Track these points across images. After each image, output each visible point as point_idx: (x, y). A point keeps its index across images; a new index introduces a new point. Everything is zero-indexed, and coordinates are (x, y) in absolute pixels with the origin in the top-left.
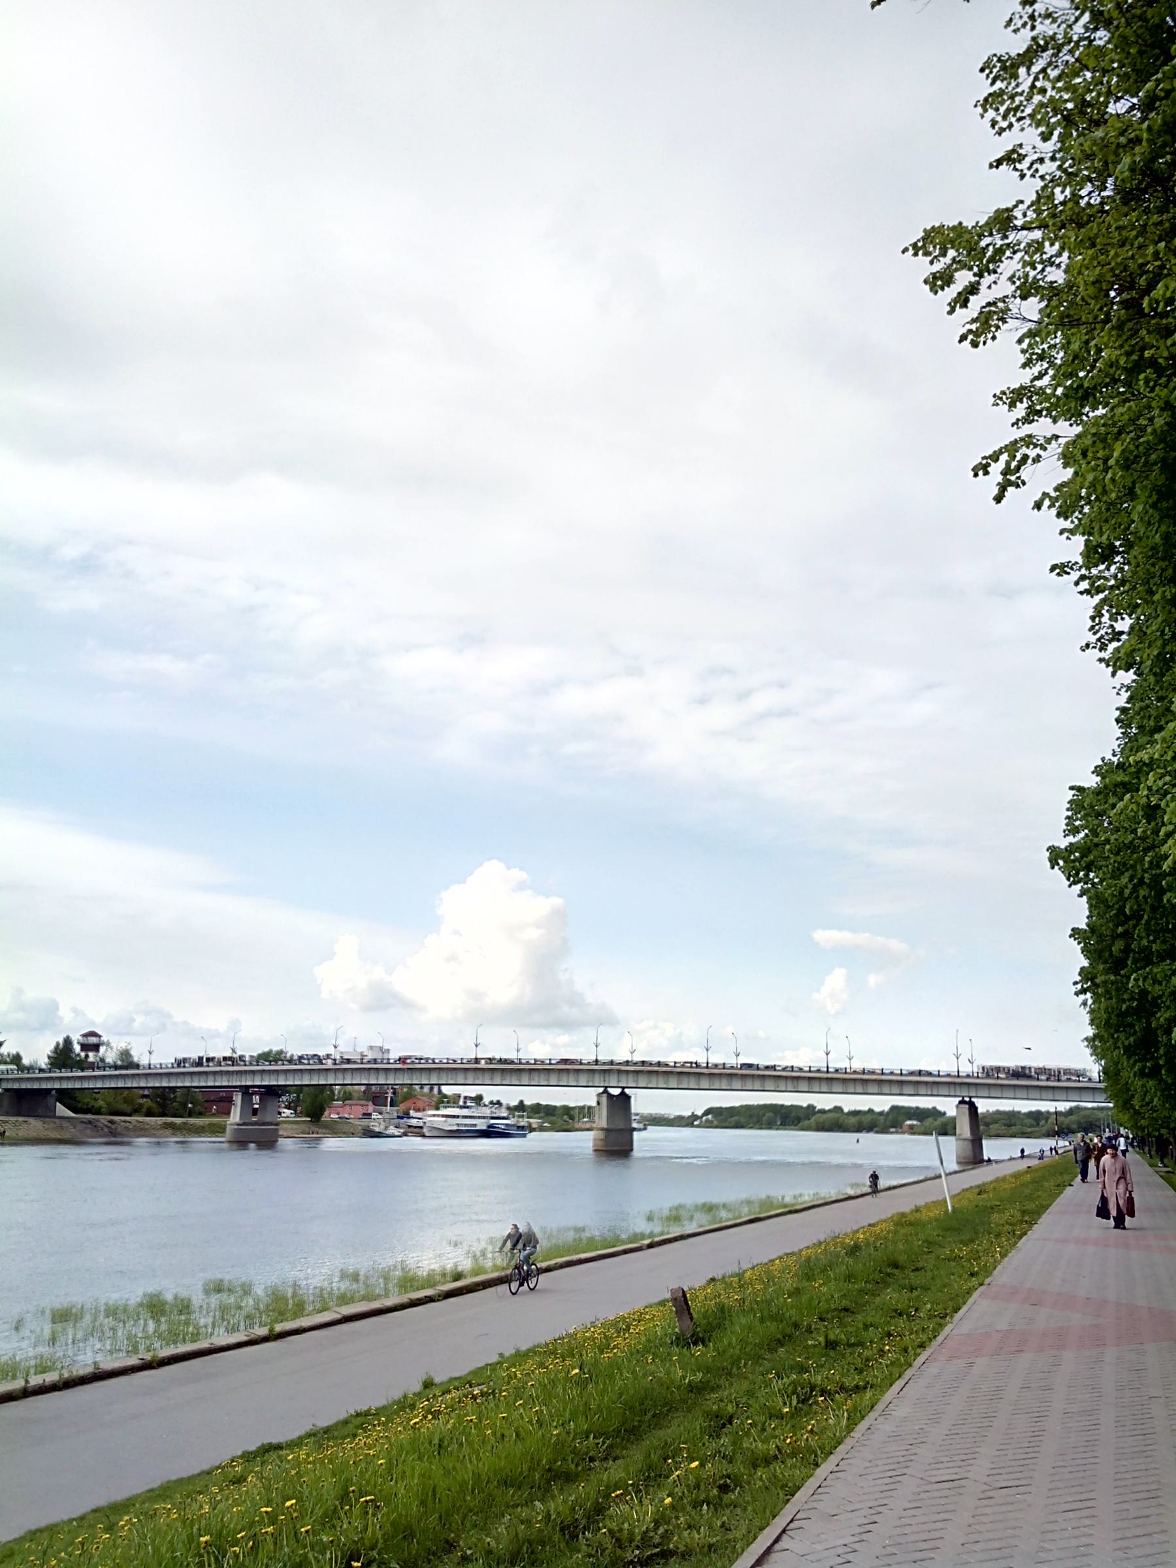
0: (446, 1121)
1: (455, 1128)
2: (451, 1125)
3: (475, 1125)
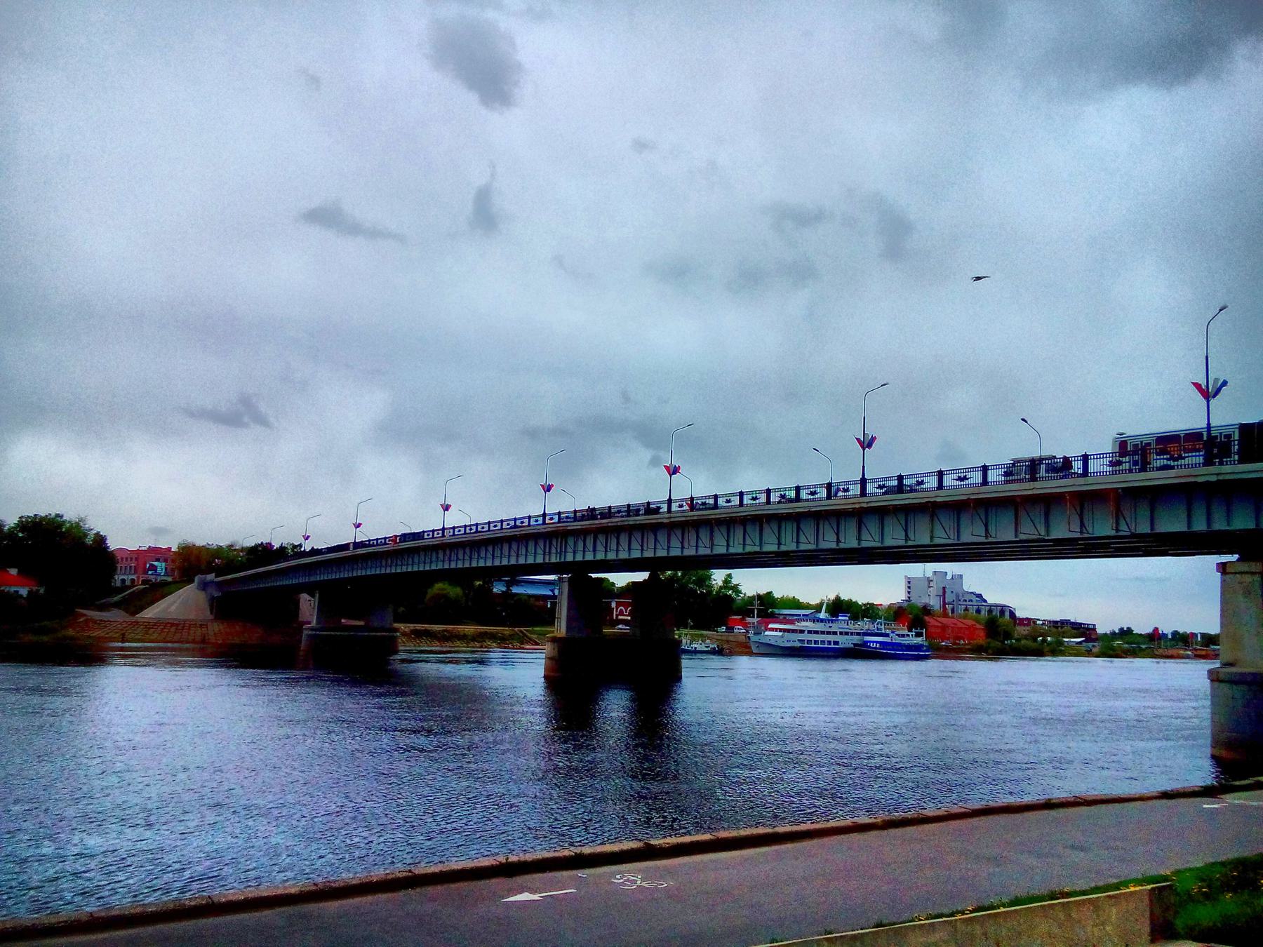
0: (782, 636)
1: (798, 645)
2: (793, 641)
3: (836, 643)
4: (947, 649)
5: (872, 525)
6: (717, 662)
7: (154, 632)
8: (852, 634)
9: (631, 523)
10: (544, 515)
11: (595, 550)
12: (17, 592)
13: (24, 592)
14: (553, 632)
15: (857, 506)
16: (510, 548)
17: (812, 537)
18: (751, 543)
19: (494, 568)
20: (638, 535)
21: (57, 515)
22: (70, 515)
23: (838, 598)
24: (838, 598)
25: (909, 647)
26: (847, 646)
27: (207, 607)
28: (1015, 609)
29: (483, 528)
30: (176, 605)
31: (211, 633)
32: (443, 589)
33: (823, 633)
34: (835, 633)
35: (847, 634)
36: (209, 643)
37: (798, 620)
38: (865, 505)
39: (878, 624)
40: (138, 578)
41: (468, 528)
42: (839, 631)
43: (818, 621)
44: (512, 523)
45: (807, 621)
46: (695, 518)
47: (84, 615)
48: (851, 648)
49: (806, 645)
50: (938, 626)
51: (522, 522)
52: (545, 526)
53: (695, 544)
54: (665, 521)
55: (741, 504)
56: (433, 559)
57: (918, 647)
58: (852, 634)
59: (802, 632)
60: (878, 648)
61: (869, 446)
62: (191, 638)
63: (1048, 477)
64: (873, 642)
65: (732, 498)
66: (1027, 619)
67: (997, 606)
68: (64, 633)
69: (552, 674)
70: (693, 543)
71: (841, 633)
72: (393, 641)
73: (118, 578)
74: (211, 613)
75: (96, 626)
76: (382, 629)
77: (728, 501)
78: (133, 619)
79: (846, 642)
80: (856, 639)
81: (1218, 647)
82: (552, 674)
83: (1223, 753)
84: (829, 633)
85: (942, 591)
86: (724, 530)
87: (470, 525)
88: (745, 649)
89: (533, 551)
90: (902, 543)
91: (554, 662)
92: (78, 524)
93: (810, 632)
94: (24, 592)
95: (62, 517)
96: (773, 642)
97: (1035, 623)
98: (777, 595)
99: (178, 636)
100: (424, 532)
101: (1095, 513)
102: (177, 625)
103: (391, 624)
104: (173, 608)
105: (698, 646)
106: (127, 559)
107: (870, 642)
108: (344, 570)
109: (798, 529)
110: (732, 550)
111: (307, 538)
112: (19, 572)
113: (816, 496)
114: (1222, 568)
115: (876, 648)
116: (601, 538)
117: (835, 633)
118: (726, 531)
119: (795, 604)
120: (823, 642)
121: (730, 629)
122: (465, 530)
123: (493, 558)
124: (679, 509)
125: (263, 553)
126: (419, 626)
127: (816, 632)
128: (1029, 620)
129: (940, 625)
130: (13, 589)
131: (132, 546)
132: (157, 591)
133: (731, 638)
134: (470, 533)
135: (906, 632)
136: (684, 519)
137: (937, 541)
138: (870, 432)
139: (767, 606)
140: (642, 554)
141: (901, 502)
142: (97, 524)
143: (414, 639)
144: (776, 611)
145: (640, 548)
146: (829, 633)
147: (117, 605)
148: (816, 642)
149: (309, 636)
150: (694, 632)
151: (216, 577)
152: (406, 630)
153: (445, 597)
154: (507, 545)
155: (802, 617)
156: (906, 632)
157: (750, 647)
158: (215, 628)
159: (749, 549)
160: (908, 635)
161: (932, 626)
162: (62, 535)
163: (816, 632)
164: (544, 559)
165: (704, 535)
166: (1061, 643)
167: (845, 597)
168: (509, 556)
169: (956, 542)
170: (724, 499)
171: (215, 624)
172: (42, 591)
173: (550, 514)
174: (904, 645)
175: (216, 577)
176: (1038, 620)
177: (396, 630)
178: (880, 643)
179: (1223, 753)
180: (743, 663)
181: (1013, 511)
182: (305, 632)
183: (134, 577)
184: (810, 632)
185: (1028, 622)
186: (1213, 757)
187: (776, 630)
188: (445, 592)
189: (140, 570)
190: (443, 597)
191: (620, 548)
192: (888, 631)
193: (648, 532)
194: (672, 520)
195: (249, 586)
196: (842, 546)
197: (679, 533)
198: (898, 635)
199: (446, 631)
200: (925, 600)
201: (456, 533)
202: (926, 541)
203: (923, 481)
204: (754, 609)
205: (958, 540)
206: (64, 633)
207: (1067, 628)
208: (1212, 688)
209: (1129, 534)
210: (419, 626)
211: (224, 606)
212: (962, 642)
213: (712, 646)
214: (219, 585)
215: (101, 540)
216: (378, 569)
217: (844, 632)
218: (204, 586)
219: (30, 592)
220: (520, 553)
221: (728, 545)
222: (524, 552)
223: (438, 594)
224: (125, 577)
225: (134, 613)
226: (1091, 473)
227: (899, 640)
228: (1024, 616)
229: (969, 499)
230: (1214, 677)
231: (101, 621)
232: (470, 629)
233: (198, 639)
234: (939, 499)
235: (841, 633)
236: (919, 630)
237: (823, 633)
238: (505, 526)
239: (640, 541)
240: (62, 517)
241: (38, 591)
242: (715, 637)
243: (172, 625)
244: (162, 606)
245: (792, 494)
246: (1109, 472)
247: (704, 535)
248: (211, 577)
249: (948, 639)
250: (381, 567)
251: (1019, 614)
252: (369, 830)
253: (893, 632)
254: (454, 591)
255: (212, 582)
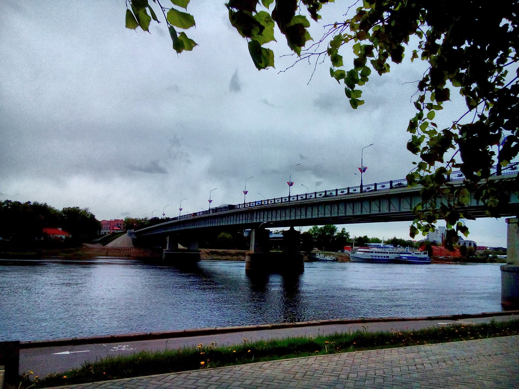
0: (363, 254)
1: (371, 258)
2: (368, 256)
3: (388, 257)
4: (441, 259)
5: (366, 205)
6: (338, 265)
7: (110, 252)
8: (395, 253)
9: (275, 206)
10: (289, 197)
11: (276, 217)
12: (61, 237)
13: (64, 237)
14: (249, 252)
15: (359, 197)
16: (276, 213)
17: (397, 207)
18: (365, 211)
19: (243, 224)
20: (293, 210)
21: (77, 207)
22: (82, 207)
23: (395, 238)
24: (395, 238)
25: (421, 259)
26: (393, 258)
27: (131, 242)
28: (476, 242)
29: (278, 201)
30: (120, 242)
31: (132, 252)
32: (224, 235)
33: (381, 253)
34: (387, 253)
35: (392, 253)
36: (131, 256)
37: (371, 247)
38: (362, 197)
39: (407, 249)
40: (110, 231)
41: (251, 204)
42: (389, 252)
43: (379, 248)
44: (304, 197)
45: (375, 248)
46: (299, 204)
47: (86, 246)
48: (394, 259)
49: (374, 258)
50: (438, 250)
51: (311, 196)
52: (245, 208)
53: (300, 215)
54: (288, 205)
55: (316, 197)
56: (201, 223)
57: (425, 259)
58: (395, 253)
59: (372, 252)
60: (406, 259)
61: (364, 171)
62: (124, 255)
63: (513, 172)
64: (404, 256)
65: (357, 189)
66: (483, 247)
67: (468, 241)
68: (77, 252)
69: (249, 269)
70: (336, 211)
71: (390, 253)
72: (199, 255)
73: (103, 231)
74: (133, 245)
75: (89, 250)
76: (194, 251)
77: (355, 190)
78: (103, 247)
79: (392, 256)
80: (397, 255)
81: (506, 256)
82: (249, 269)
83: (505, 303)
84: (384, 253)
85: (442, 234)
86: (351, 205)
87: (264, 201)
88: (347, 259)
89: (275, 216)
90: (378, 212)
91: (249, 264)
92: (85, 210)
93: (376, 252)
94: (64, 237)
95: (79, 208)
96: (360, 257)
97: (486, 248)
98: (370, 237)
99: (119, 254)
100: (196, 213)
101: (384, 205)
102: (119, 249)
103: (198, 249)
104: (119, 243)
105: (328, 258)
106: (106, 224)
107: (403, 256)
108: (202, 224)
109: (362, 206)
110: (314, 217)
111: (164, 215)
112: (62, 230)
113: (343, 193)
114: (508, 221)
115: (405, 259)
116: (293, 210)
117: (387, 253)
118: (378, 203)
119: (377, 241)
120: (382, 257)
121: (343, 251)
122: (250, 205)
123: (220, 223)
124: (341, 194)
125: (155, 220)
126: (213, 250)
127: (379, 252)
128: (483, 247)
129: (439, 249)
130: (59, 236)
131: (108, 218)
132: (114, 236)
133: (343, 255)
134: (253, 206)
135: (420, 252)
136: (294, 204)
137: (391, 211)
138: (364, 165)
139: (363, 242)
140: (281, 219)
141: (376, 195)
142: (92, 211)
143: (211, 255)
144: (368, 244)
145: (311, 214)
146: (384, 253)
147: (99, 242)
148: (379, 257)
149: (166, 253)
150: (326, 252)
151: (134, 231)
152: (208, 251)
153: (225, 238)
154: (263, 213)
155: (373, 246)
156: (420, 252)
157: (350, 259)
158: (133, 250)
159: (320, 216)
160: (421, 254)
161: (435, 250)
162: (80, 215)
163: (379, 252)
164: (245, 222)
165: (342, 208)
166: (496, 257)
167: (398, 238)
168: (242, 220)
169: (399, 211)
170: (353, 190)
171: (134, 249)
172: (70, 236)
173: (292, 197)
174: (419, 258)
175: (134, 231)
176: (488, 247)
177: (200, 251)
178: (407, 257)
179: (505, 303)
180: (348, 265)
181: (368, 204)
182: (164, 252)
183: (109, 231)
184: (376, 252)
185: (483, 248)
186: (502, 304)
187: (361, 251)
188: (225, 236)
189: (111, 229)
190: (224, 238)
191: (286, 216)
192: (411, 252)
193: (334, 206)
194: (290, 205)
195: (152, 232)
196: (355, 214)
197: (329, 207)
198: (416, 254)
199: (224, 252)
200: (435, 239)
201: (246, 206)
202: (387, 211)
203: (384, 185)
204: (353, 243)
205: (400, 211)
206: (77, 252)
207: (501, 251)
208: (502, 275)
209: (468, 206)
210: (213, 250)
211: (137, 242)
212: (450, 257)
213: (333, 258)
214: (136, 234)
215: (93, 217)
216: (199, 226)
217: (392, 252)
218: (130, 234)
219: (66, 237)
220: (282, 216)
221: (312, 215)
222: (270, 216)
223: (222, 237)
224: (106, 231)
225: (104, 245)
226: (503, 173)
227: (416, 256)
228: (481, 246)
229: (402, 193)
230: (503, 269)
231: (91, 248)
232: (233, 251)
233: (127, 254)
234: (390, 193)
235: (390, 253)
236: (425, 252)
237: (381, 253)
238: (269, 203)
239: (352, 207)
240: (79, 208)
241: (69, 236)
242: (336, 254)
243: (117, 249)
244: (115, 242)
245: (373, 188)
246: (510, 173)
247: (342, 208)
248: (133, 231)
249: (443, 255)
250: (215, 222)
251: (478, 245)
252: (166, 313)
253: (413, 252)
254: (229, 236)
255: (133, 233)
